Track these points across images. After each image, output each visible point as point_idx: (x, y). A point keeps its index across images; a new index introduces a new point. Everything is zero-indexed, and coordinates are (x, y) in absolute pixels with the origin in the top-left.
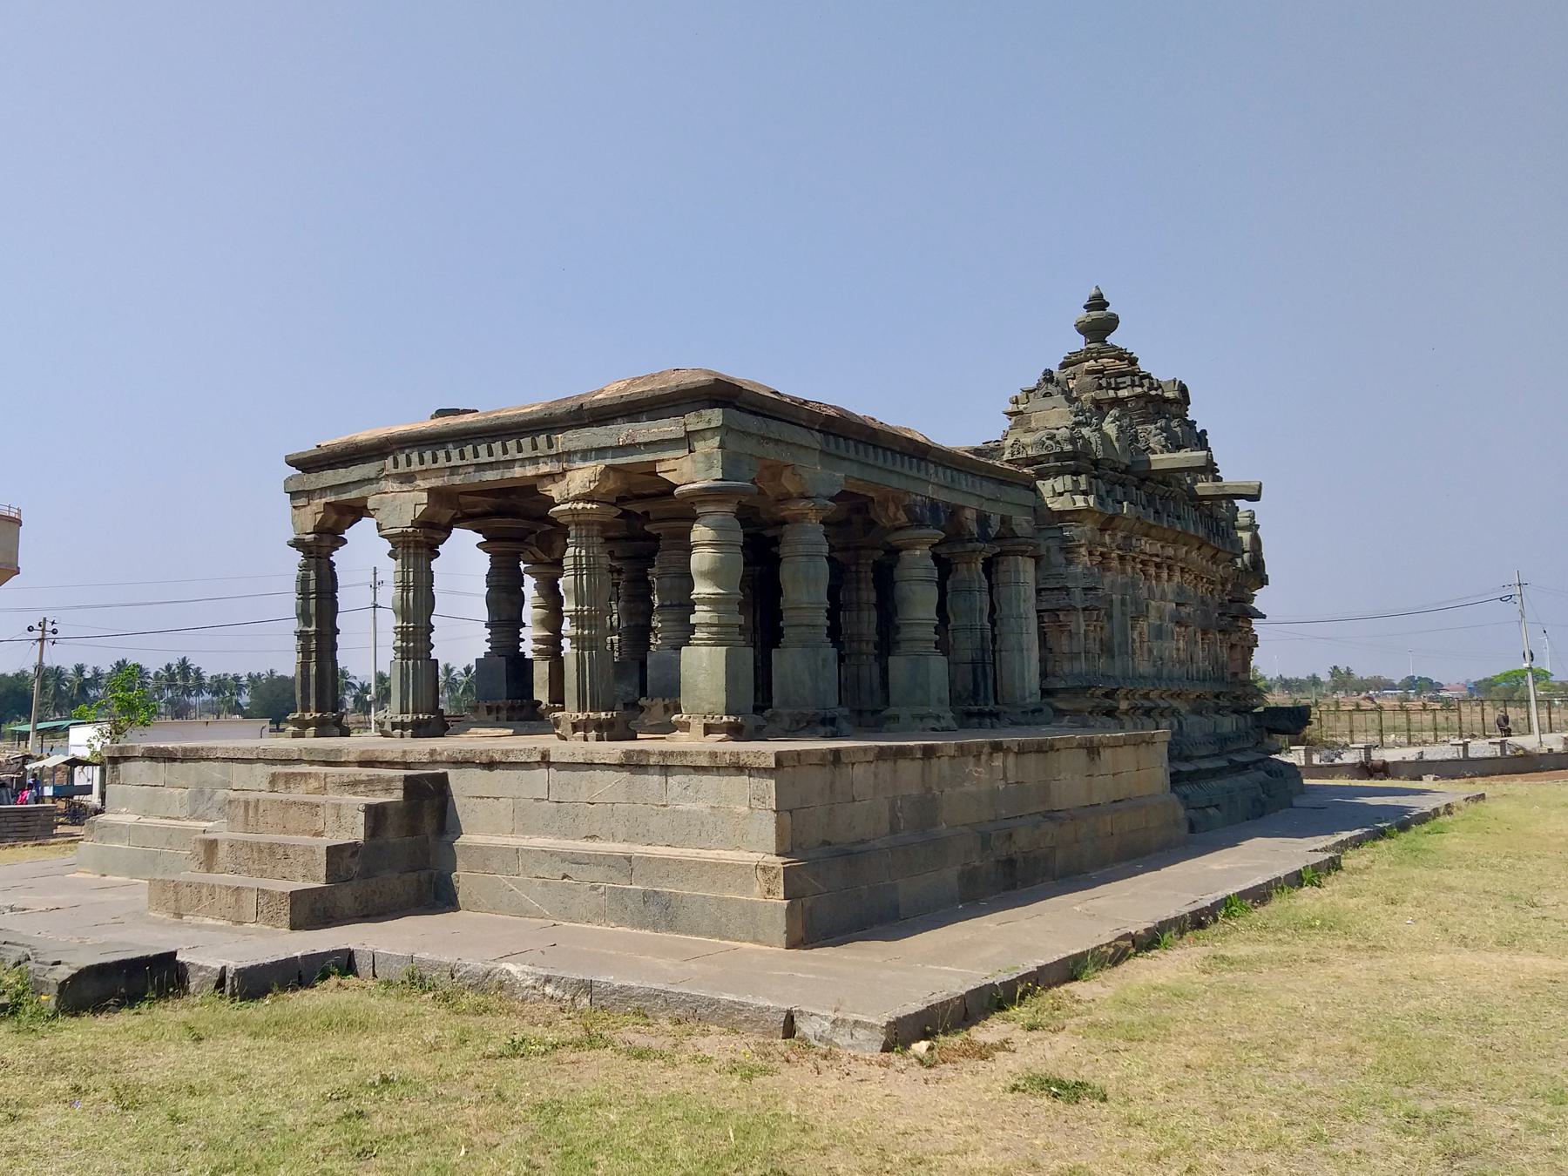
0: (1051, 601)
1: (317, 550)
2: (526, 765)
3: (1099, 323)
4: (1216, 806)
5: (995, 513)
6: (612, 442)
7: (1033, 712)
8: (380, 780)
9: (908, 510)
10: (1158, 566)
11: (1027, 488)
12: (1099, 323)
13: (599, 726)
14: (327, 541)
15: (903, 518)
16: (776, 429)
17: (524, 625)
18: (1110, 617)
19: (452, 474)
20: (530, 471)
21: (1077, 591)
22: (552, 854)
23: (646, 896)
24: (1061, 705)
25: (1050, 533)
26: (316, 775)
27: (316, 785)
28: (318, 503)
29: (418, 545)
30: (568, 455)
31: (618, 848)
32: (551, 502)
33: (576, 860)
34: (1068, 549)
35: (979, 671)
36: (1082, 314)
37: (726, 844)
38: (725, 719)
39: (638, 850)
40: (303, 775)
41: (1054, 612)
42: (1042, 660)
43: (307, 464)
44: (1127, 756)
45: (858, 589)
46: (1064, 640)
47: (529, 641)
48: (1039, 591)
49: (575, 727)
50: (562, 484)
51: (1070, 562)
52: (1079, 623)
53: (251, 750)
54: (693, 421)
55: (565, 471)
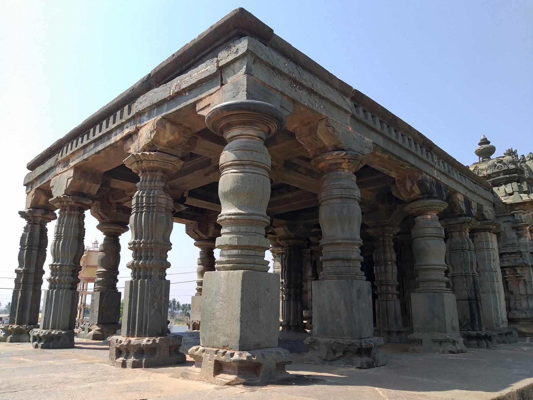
0: (510, 261)
5: (475, 200)
7: (506, 334)
9: (421, 184)
13: (140, 351)
15: (417, 191)
16: (306, 78)
21: (528, 254)
25: (505, 219)
29: (72, 208)
30: (140, 114)
34: (518, 228)
35: (474, 306)
36: (479, 147)
38: (236, 356)
41: (513, 268)
42: (507, 300)
45: (385, 252)
46: (521, 286)
48: (501, 255)
51: (520, 236)
54: (225, 57)
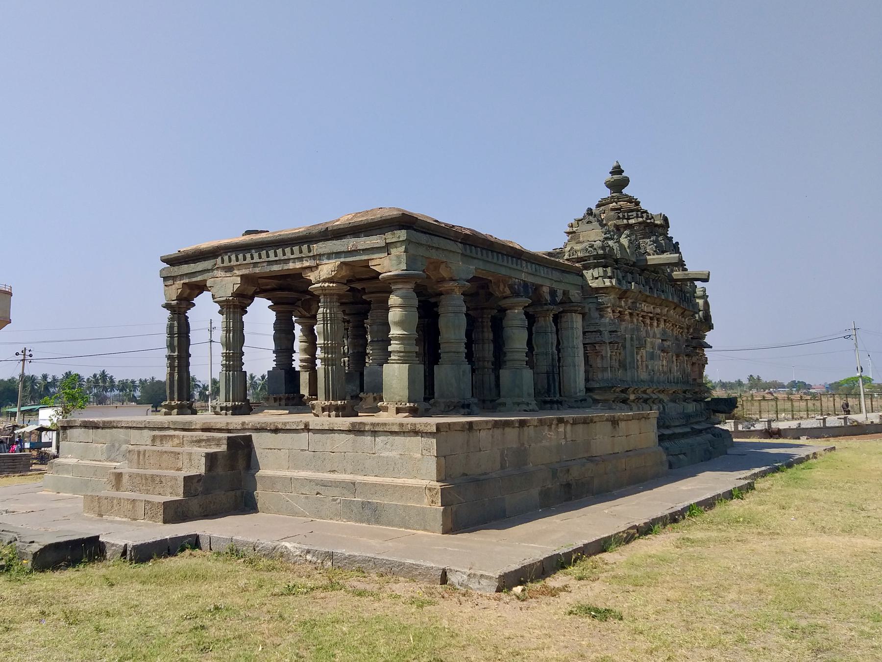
0: (591, 338)
1: (179, 310)
2: (296, 431)
3: (618, 182)
4: (684, 454)
5: (560, 289)
6: (344, 249)
7: (581, 401)
8: (214, 439)
9: (511, 287)
10: (651, 318)
11: (578, 275)
12: (618, 182)
13: (337, 409)
14: (184, 304)
15: (508, 292)
16: (436, 241)
17: (295, 352)
18: (624, 347)
19: (254, 267)
20: (298, 265)
21: (606, 333)
22: (311, 481)
23: (363, 505)
24: (597, 397)
25: (591, 300)
26: (178, 437)
27: (178, 442)
28: (179, 283)
29: (235, 307)
30: (320, 256)
31: (348, 477)
32: (310, 283)
33: (324, 484)
34: (601, 309)
35: (551, 377)
36: (609, 177)
37: (408, 475)
38: (408, 405)
39: (359, 478)
40: (171, 436)
41: (593, 344)
42: (586, 372)
43: (173, 261)
44: (634, 426)
45: (483, 332)
46: (599, 360)
47: (298, 361)
48: (584, 333)
49: (324, 409)
50: (316, 273)
51: (602, 316)
52: (607, 351)
53: (141, 422)
54: (390, 237)
55: (318, 265)
